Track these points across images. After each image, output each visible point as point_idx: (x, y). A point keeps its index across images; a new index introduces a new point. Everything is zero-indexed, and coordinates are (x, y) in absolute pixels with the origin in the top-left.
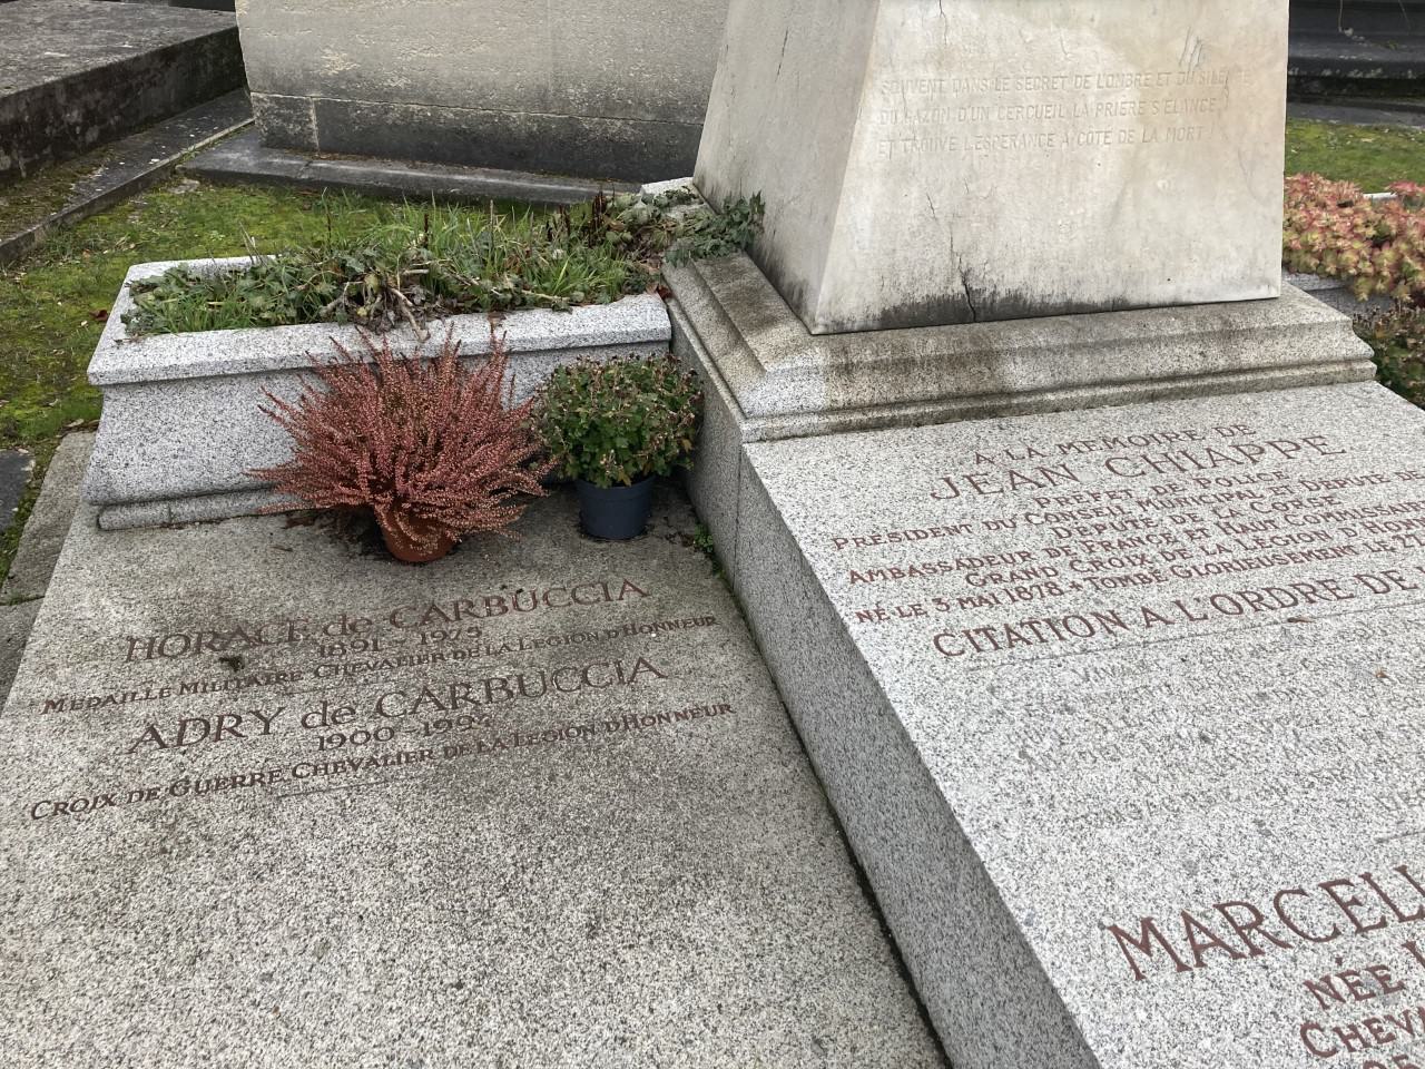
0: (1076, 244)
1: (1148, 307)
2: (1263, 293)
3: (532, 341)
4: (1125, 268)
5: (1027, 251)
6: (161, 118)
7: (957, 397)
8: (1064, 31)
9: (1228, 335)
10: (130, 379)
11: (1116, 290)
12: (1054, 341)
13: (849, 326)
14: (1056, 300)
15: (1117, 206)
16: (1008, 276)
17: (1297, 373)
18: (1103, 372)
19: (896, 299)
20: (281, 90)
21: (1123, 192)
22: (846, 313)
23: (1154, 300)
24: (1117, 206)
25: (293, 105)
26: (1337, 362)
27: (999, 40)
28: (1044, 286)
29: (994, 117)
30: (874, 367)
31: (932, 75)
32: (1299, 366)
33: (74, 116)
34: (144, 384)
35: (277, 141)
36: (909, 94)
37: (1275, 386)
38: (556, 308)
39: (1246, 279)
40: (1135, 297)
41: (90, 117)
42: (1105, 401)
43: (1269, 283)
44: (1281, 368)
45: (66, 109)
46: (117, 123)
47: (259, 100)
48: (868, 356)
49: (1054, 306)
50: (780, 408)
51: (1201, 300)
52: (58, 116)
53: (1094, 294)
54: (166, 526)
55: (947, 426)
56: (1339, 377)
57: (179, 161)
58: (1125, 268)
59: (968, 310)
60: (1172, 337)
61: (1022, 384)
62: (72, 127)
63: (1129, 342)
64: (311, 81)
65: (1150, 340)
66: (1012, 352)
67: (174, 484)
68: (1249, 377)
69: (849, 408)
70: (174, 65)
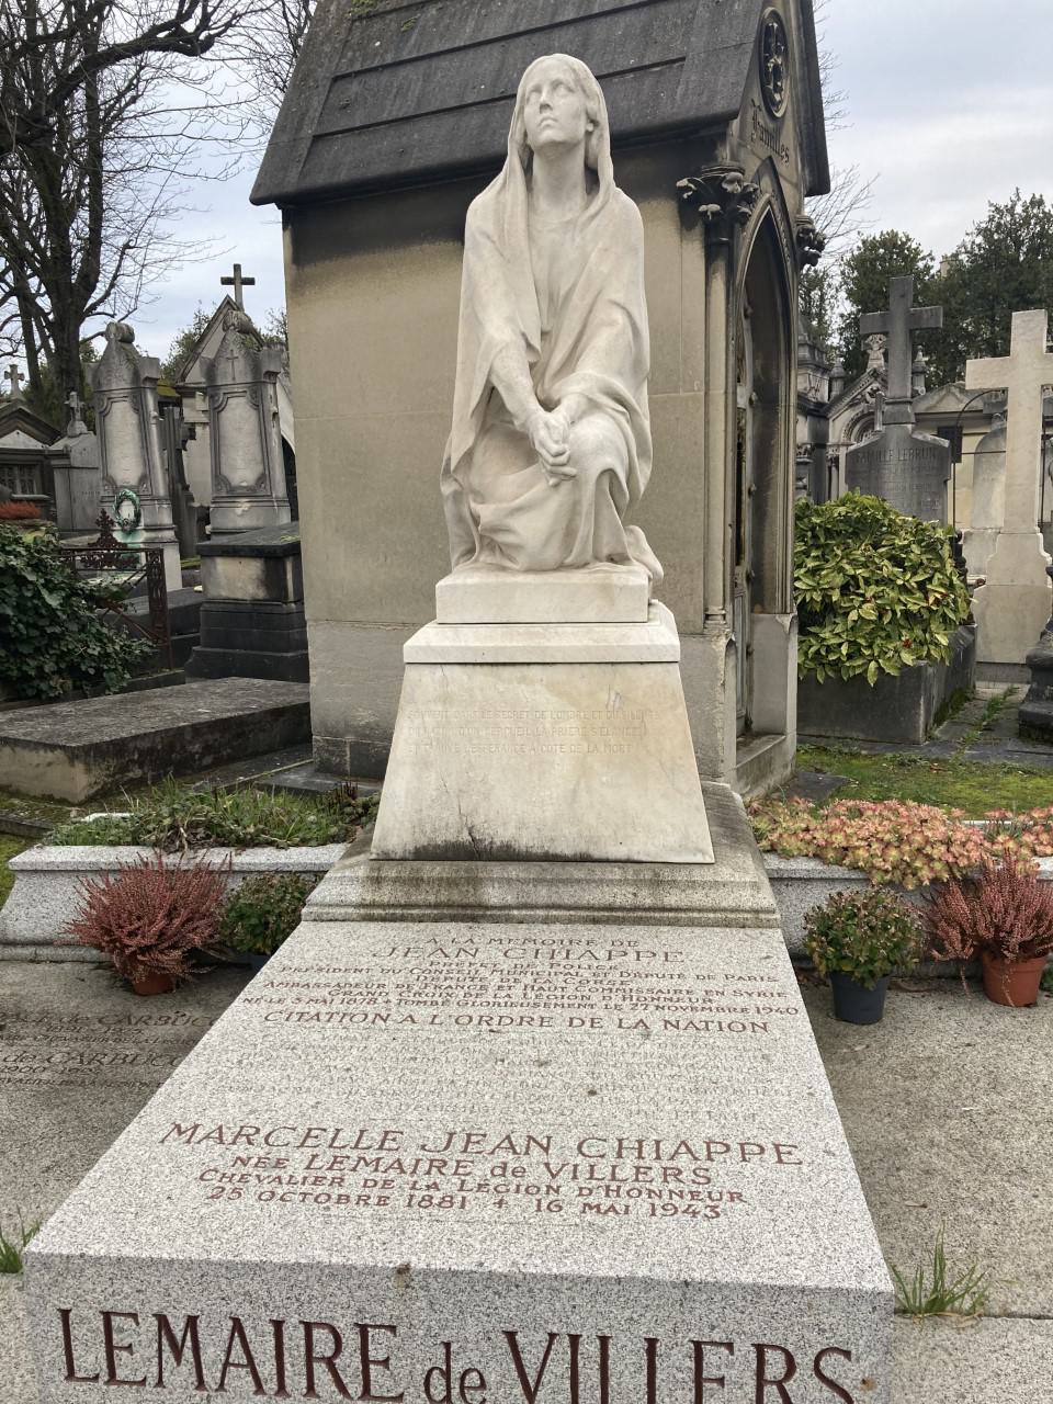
0: (547, 814)
1: (607, 861)
2: (699, 858)
3: (255, 864)
4: (586, 833)
5: (512, 815)
6: (265, 753)
7: (449, 906)
8: (523, 686)
9: (657, 883)
10: (29, 867)
11: (581, 847)
12: (522, 875)
13: (393, 856)
14: (537, 850)
15: (575, 791)
16: (501, 829)
17: (711, 915)
18: (555, 899)
19: (424, 841)
20: (330, 734)
21: (578, 783)
22: (390, 847)
23: (612, 857)
24: (575, 791)
25: (336, 744)
26: (748, 912)
27: (482, 690)
28: (526, 840)
29: (483, 733)
30: (396, 880)
31: (440, 708)
32: (714, 910)
33: (197, 747)
34: (36, 871)
35: (325, 768)
36: (427, 719)
37: (692, 923)
38: (278, 847)
39: (683, 848)
40: (596, 854)
41: (207, 749)
42: (556, 920)
43: (703, 853)
44: (700, 911)
45: (190, 743)
46: (229, 755)
47: (317, 741)
48: (393, 874)
49: (536, 854)
50: (327, 900)
51: (650, 859)
52: (183, 747)
53: (565, 848)
54: (32, 961)
55: (439, 925)
56: (749, 923)
57: (257, 779)
58: (586, 833)
59: (472, 853)
60: (611, 881)
61: (494, 901)
62: (193, 755)
63: (579, 881)
64: (348, 728)
65: (594, 881)
66: (492, 880)
67: (39, 934)
68: (671, 915)
69: (373, 905)
70: (282, 719)
